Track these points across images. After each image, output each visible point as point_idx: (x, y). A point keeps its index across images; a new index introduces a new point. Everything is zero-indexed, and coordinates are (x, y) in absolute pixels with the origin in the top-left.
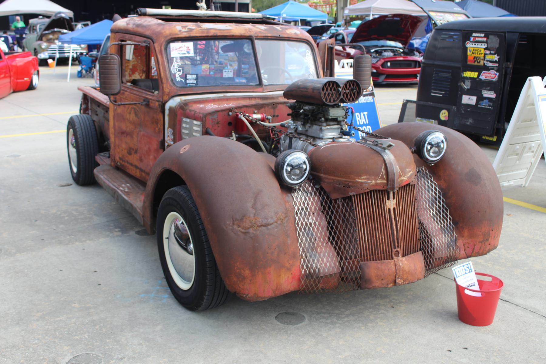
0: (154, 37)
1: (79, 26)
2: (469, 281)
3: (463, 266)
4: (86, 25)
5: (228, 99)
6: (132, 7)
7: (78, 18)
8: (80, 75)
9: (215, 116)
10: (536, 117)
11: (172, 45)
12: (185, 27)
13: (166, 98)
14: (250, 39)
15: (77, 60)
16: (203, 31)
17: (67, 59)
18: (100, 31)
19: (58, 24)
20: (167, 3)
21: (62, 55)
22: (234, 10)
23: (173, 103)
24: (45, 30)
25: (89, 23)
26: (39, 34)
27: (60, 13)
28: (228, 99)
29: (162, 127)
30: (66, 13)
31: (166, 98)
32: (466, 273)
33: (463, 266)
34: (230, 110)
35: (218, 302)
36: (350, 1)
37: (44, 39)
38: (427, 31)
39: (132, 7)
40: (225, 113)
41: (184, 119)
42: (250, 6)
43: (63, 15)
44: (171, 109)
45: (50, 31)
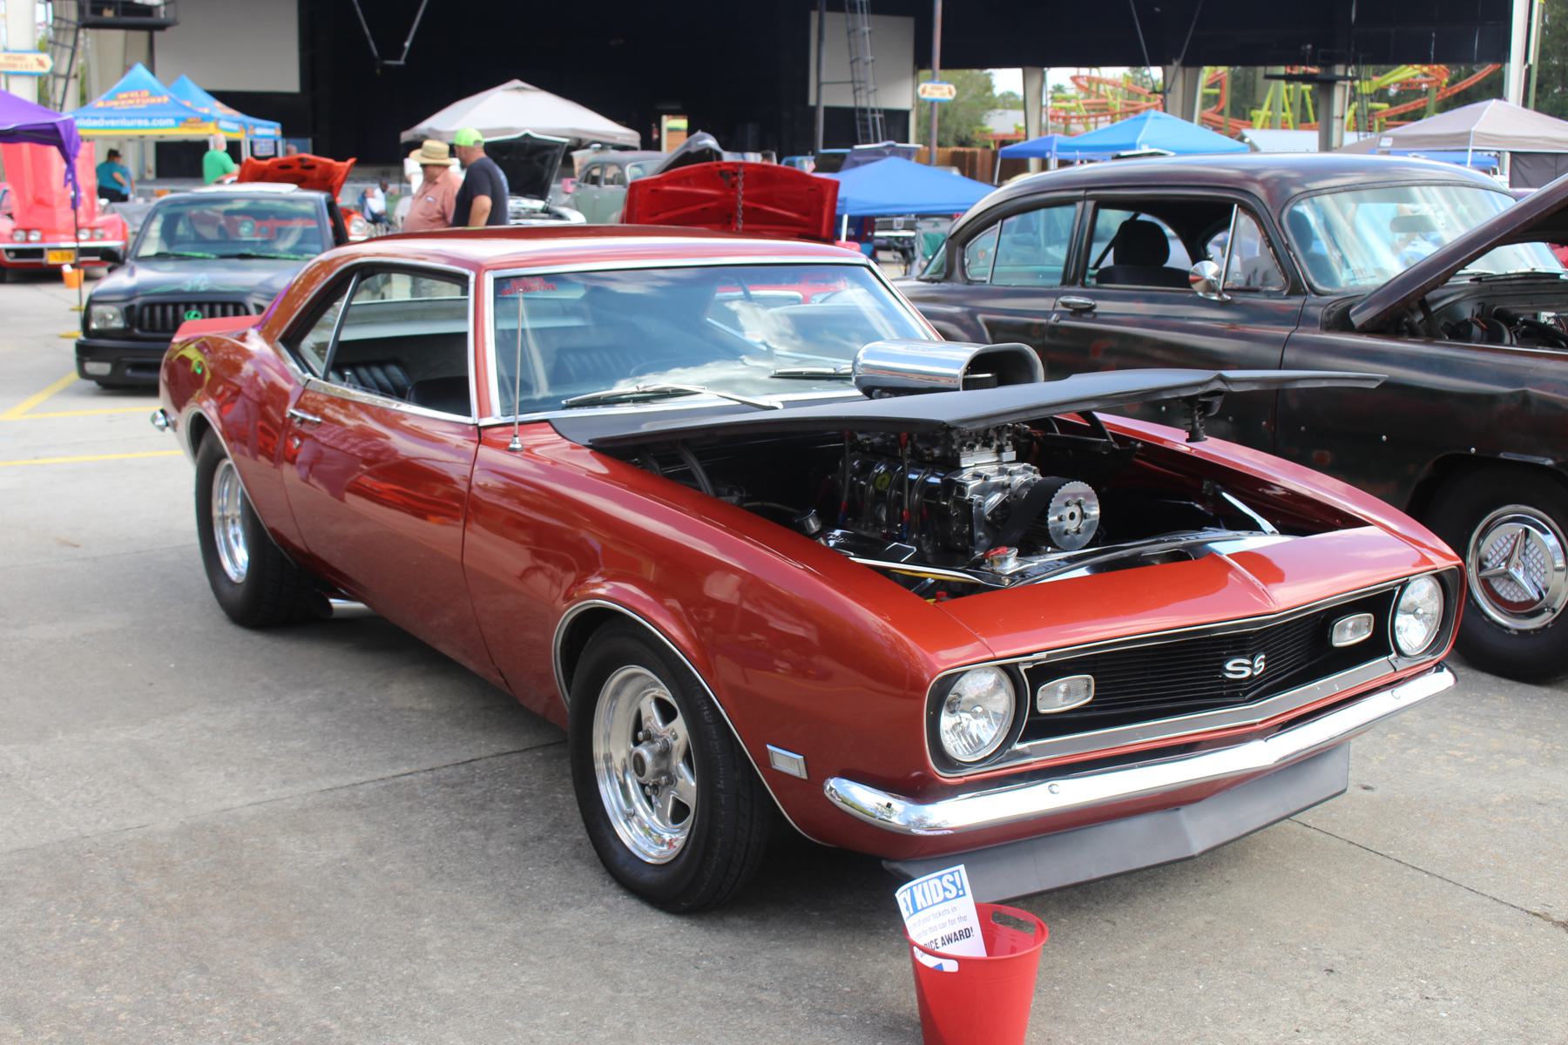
3: (940, 878)
32: (946, 899)
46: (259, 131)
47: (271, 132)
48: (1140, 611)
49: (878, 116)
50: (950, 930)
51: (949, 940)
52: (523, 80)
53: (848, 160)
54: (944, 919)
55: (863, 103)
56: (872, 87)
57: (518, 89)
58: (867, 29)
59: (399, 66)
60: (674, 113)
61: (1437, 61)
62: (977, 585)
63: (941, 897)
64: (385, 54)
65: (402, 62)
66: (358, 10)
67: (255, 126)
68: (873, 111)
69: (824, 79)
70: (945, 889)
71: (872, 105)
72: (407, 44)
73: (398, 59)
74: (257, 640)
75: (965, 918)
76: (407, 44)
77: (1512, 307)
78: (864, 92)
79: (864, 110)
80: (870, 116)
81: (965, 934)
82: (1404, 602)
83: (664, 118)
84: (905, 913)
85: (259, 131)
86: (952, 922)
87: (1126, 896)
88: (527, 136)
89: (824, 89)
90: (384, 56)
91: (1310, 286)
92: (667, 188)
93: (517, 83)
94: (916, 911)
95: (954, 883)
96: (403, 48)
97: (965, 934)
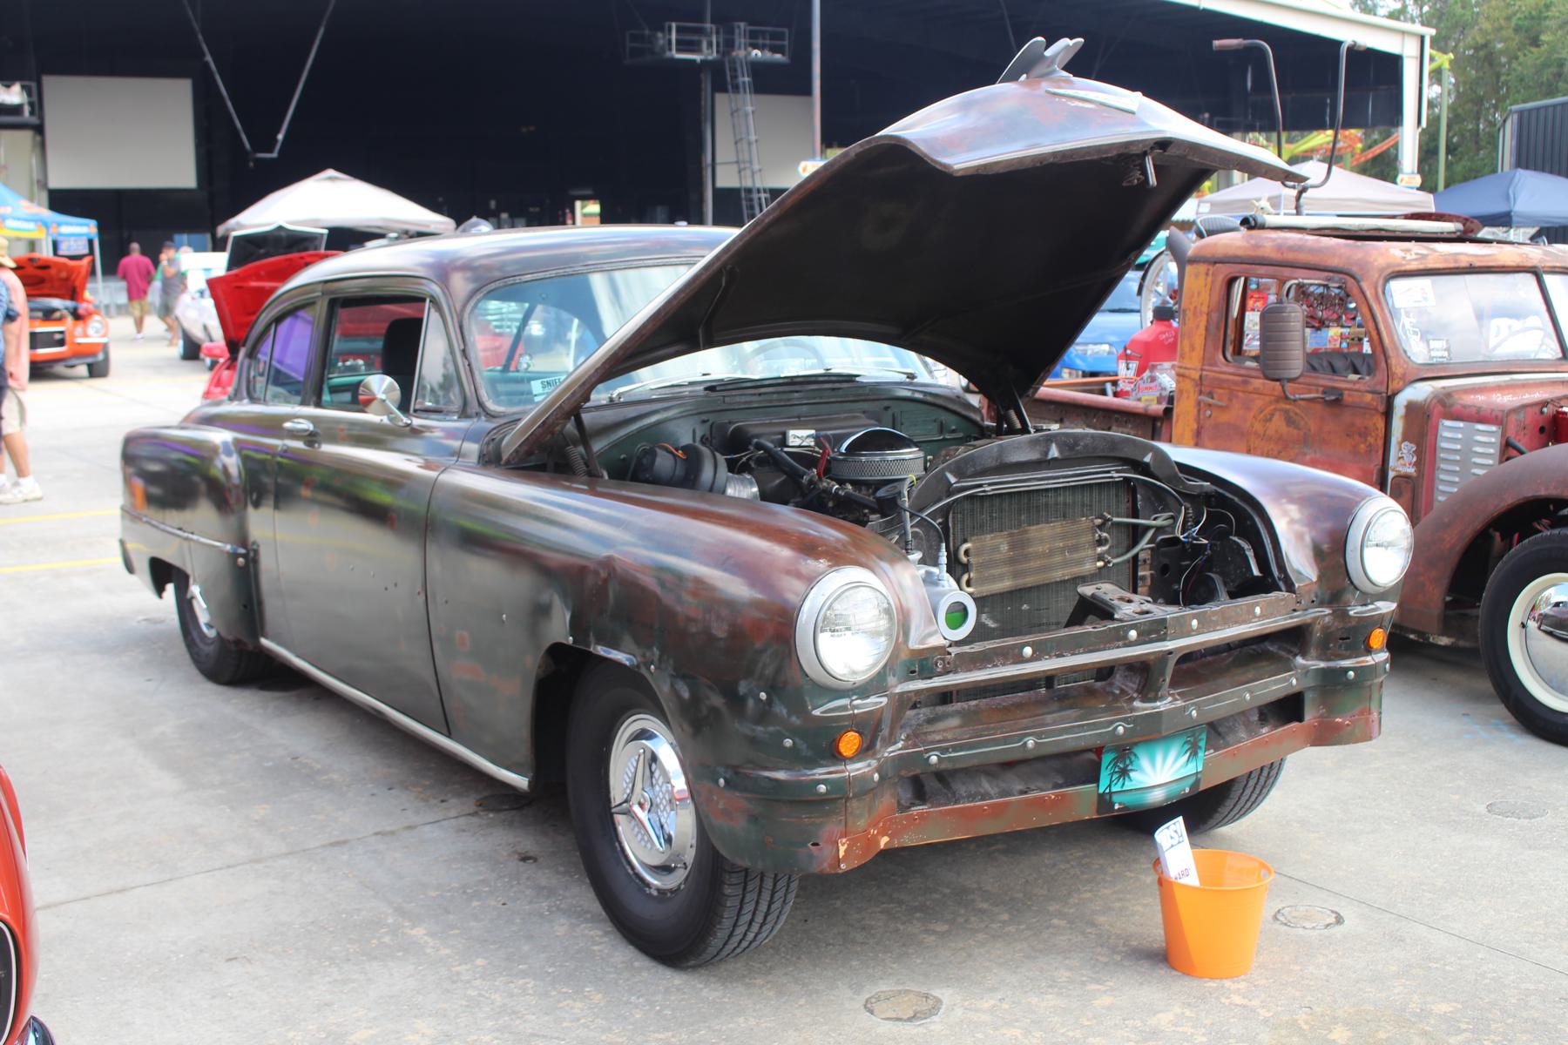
0: (1354, 270)
5: (1525, 386)
6: (493, 204)
9: (1521, 416)
11: (1395, 285)
12: (1408, 251)
13: (1394, 385)
14: (1536, 273)
16: (1445, 256)
20: (589, 192)
23: (1419, 392)
28: (1525, 386)
29: (1380, 442)
31: (1394, 385)
34: (1545, 403)
35: (763, 907)
38: (291, 247)
40: (1537, 409)
41: (1448, 423)
44: (1411, 408)
46: (65, 230)
47: (84, 230)
49: (763, 196)
55: (748, 183)
56: (756, 167)
57: (331, 179)
58: (749, 109)
59: (272, 160)
60: (584, 198)
61: (1348, 124)
64: (258, 147)
65: (275, 155)
66: (229, 104)
67: (59, 225)
68: (759, 191)
69: (718, 160)
71: (759, 184)
72: (280, 137)
73: (271, 151)
74: (211, 687)
76: (280, 137)
77: (757, 426)
78: (748, 173)
79: (749, 191)
80: (755, 196)
83: (578, 204)
85: (65, 230)
87: (961, 896)
88: (281, 228)
89: (719, 169)
90: (256, 149)
91: (481, 404)
92: (254, 284)
93: (331, 172)
96: (276, 140)
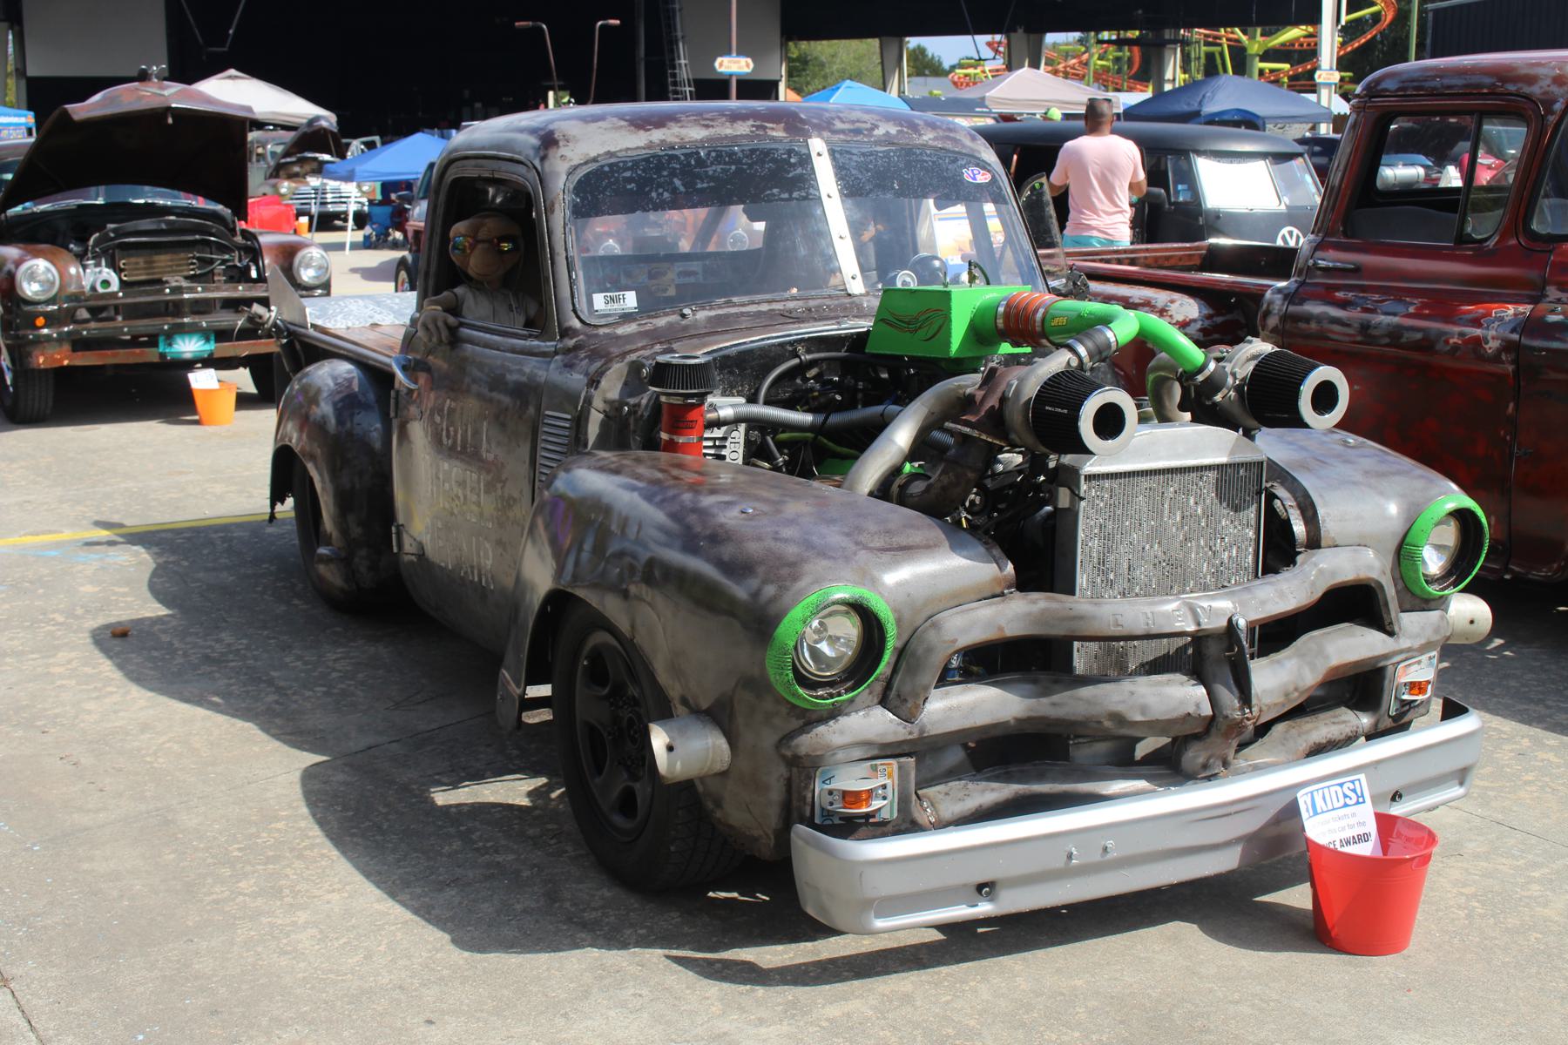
1: (356, 145)
2: (1351, 827)
3: (1341, 785)
4: (371, 146)
6: (467, 93)
7: (350, 128)
8: (368, 244)
10: (391, 141)
15: (361, 220)
17: (343, 216)
18: (415, 155)
19: (309, 140)
21: (323, 209)
22: (726, 97)
24: (286, 154)
25: (377, 138)
26: (272, 163)
27: (317, 118)
30: (327, 119)
32: (1346, 805)
33: (1341, 785)
36: (1420, 4)
37: (282, 173)
39: (467, 93)
42: (782, 87)
43: (324, 124)
45: (293, 159)
48: (73, 192)
50: (1349, 834)
51: (1348, 843)
52: (238, 69)
53: (1003, 207)
54: (1344, 823)
57: (230, 77)
62: (1202, 269)
63: (1342, 802)
70: (1345, 796)
75: (1364, 824)
81: (1364, 838)
82: (1191, 628)
84: (1304, 815)
86: (1351, 827)
93: (232, 72)
94: (1316, 813)
95: (1354, 791)
97: (1364, 838)
